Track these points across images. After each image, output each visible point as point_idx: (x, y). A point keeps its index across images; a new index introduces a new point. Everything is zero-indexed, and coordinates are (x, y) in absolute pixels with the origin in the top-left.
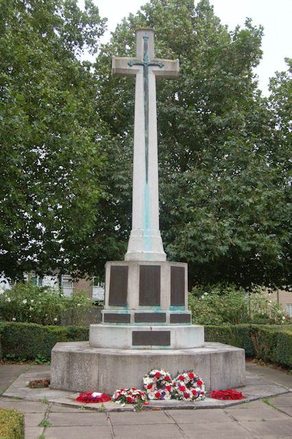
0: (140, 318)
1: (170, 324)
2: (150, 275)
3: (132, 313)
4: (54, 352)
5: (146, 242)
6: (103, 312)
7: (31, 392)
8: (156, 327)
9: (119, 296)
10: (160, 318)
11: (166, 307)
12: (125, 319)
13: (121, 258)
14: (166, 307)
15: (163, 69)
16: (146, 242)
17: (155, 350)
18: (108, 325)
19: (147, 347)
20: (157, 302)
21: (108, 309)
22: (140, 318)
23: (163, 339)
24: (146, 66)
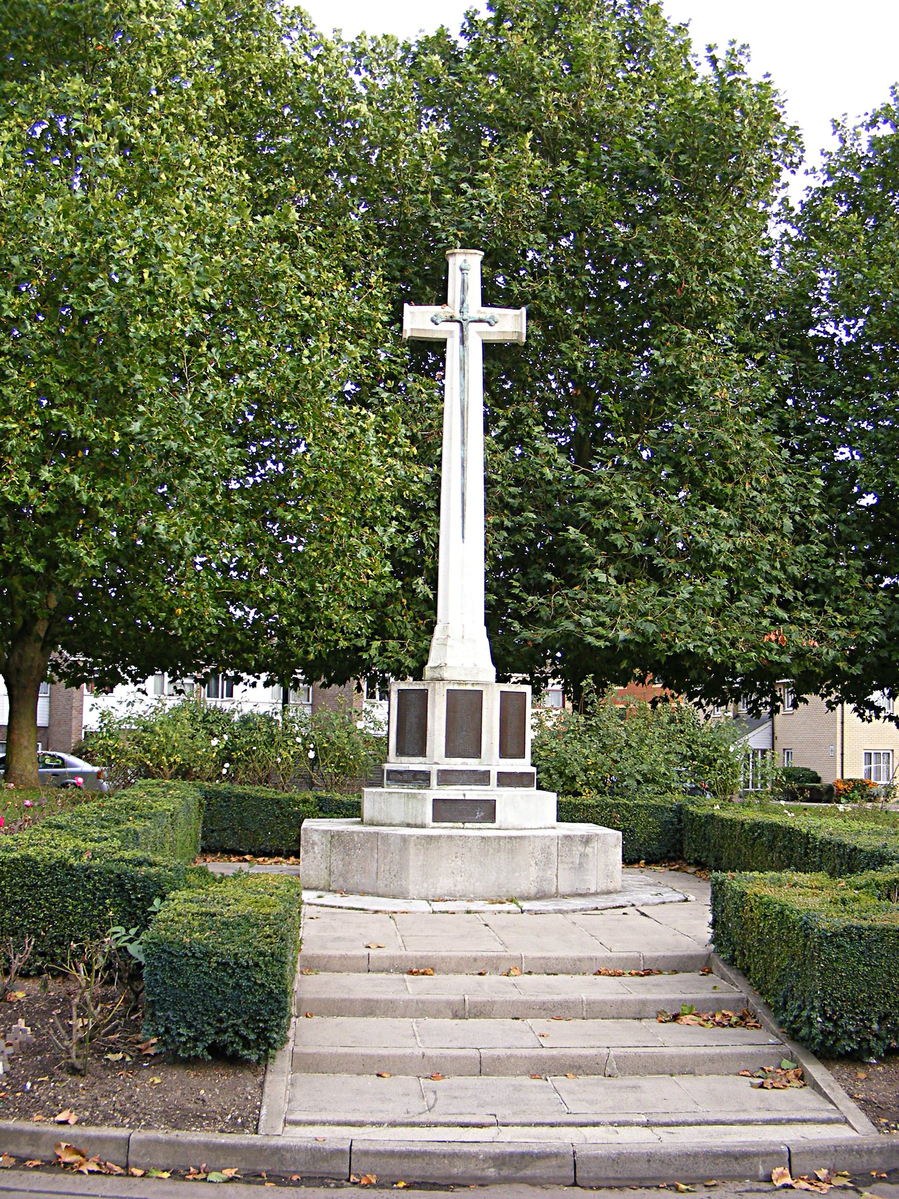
0: (446, 777)
1: (496, 788)
2: (465, 706)
3: (434, 769)
4: (305, 829)
5: (461, 647)
6: (387, 767)
7: (446, 628)
8: (474, 793)
9: (413, 738)
10: (482, 778)
11: (492, 760)
12: (421, 779)
13: (418, 675)
14: (492, 760)
15: (496, 328)
16: (461, 647)
17: (473, 830)
18: (395, 789)
19: (456, 825)
20: (421, 751)
21: (395, 763)
22: (446, 777)
23: (487, 811)
24: (464, 323)
